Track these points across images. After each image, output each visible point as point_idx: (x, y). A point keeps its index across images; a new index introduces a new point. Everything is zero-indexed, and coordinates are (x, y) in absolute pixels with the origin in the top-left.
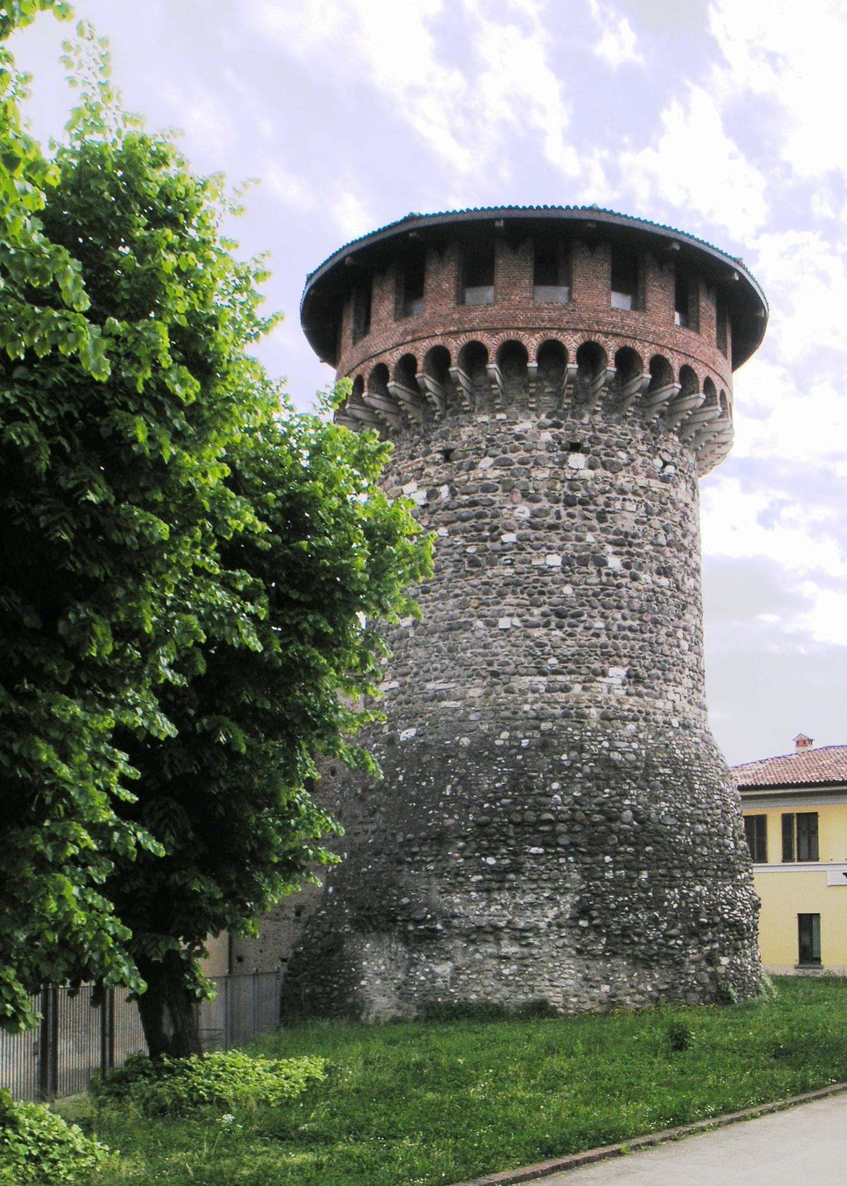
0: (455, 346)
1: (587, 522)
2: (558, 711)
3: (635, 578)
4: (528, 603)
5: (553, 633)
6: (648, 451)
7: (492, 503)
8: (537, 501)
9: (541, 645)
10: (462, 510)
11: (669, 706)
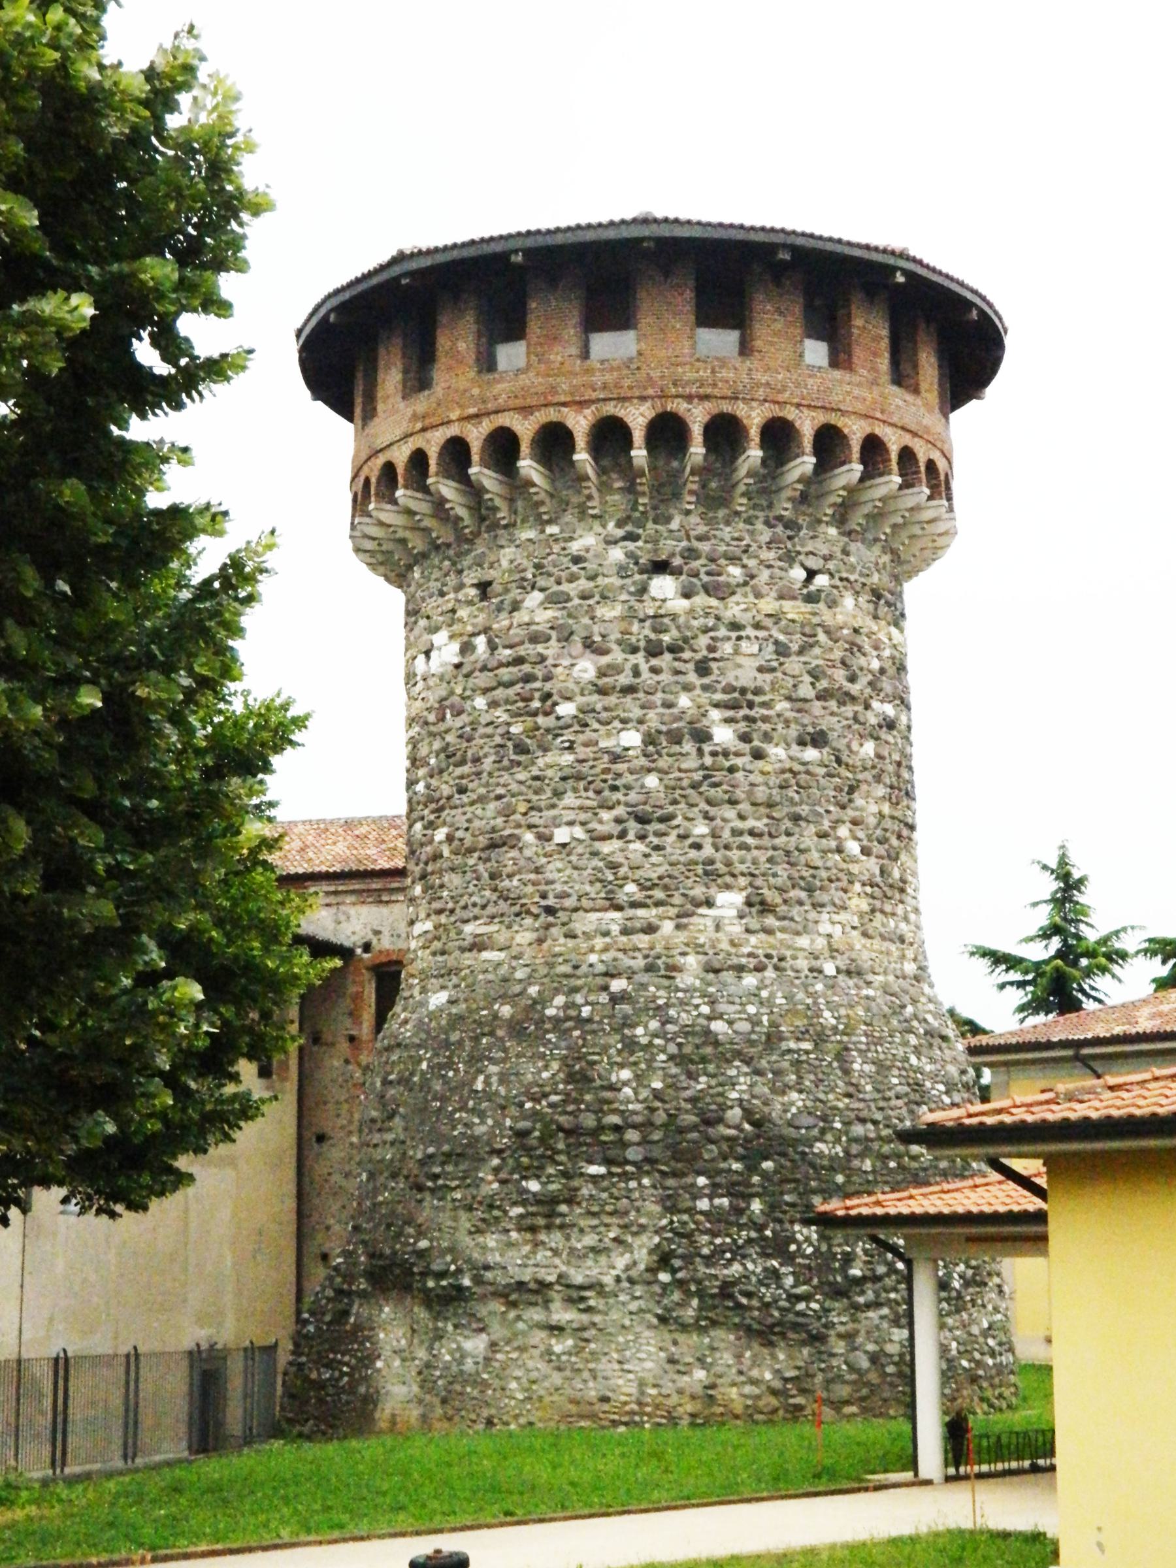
0: (476, 435)
1: (680, 678)
2: (640, 963)
3: (758, 755)
4: (595, 804)
5: (632, 846)
6: (780, 559)
7: (543, 659)
8: (604, 652)
9: (614, 866)
10: (503, 670)
11: (821, 943)
